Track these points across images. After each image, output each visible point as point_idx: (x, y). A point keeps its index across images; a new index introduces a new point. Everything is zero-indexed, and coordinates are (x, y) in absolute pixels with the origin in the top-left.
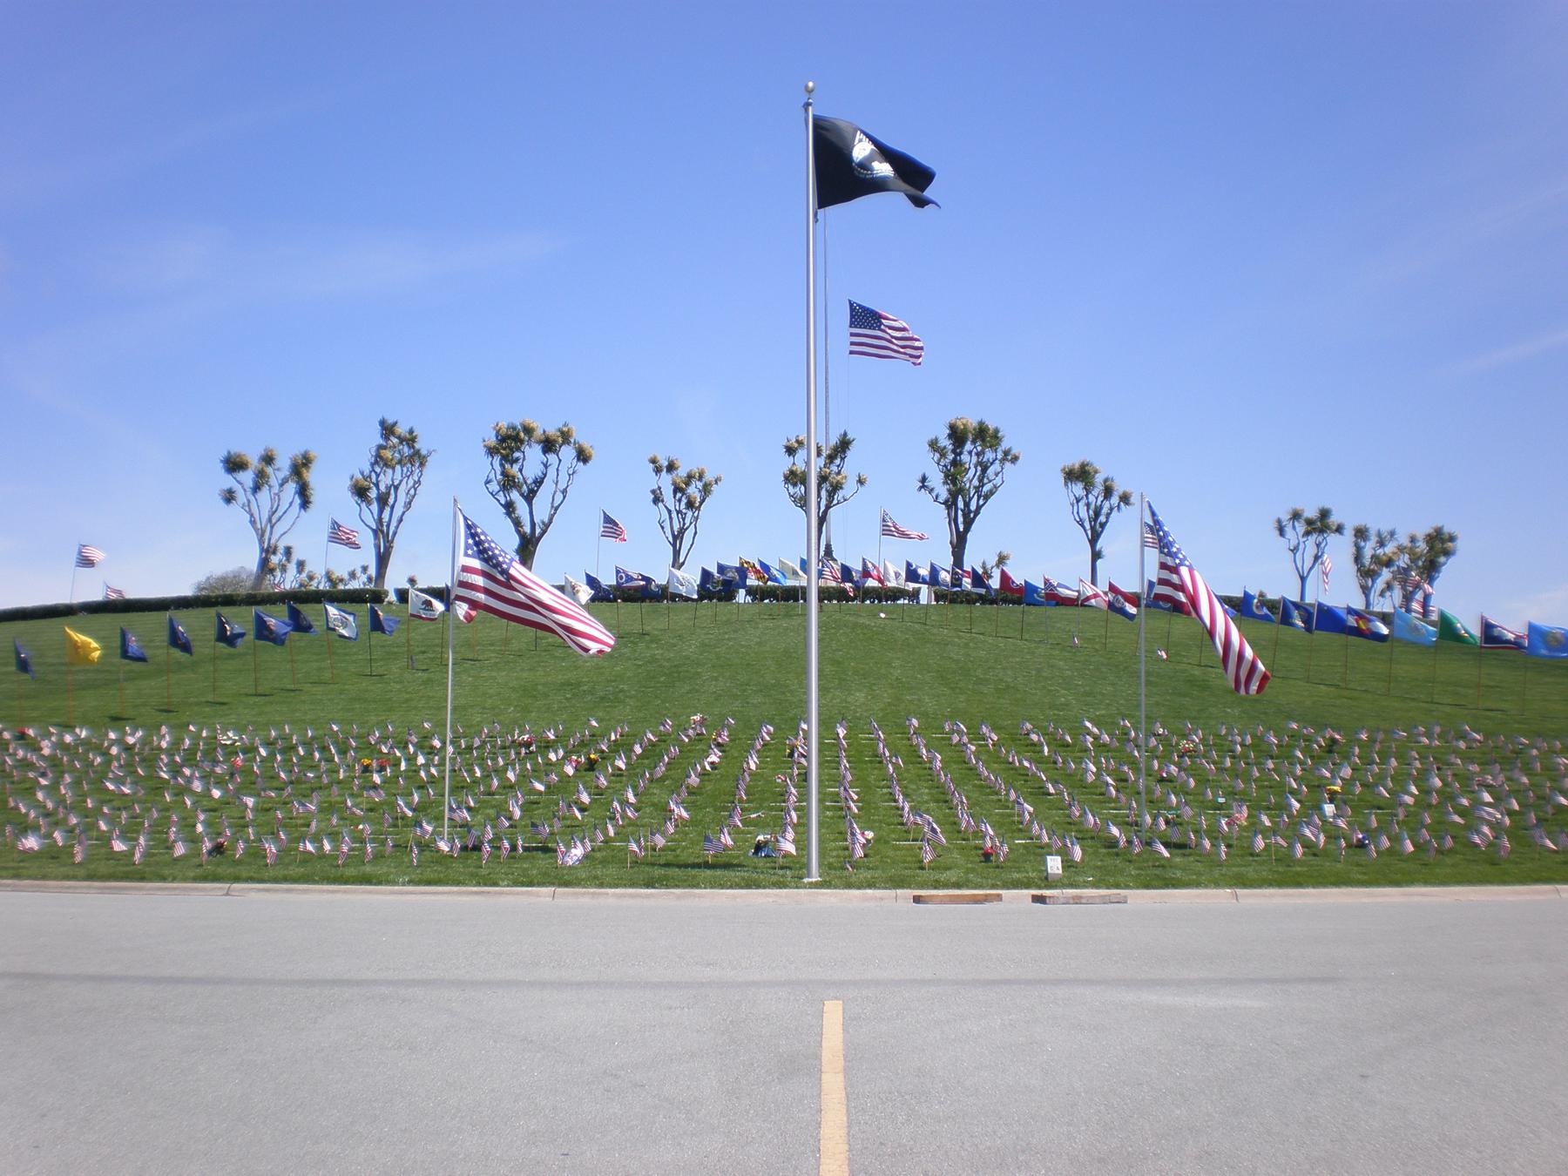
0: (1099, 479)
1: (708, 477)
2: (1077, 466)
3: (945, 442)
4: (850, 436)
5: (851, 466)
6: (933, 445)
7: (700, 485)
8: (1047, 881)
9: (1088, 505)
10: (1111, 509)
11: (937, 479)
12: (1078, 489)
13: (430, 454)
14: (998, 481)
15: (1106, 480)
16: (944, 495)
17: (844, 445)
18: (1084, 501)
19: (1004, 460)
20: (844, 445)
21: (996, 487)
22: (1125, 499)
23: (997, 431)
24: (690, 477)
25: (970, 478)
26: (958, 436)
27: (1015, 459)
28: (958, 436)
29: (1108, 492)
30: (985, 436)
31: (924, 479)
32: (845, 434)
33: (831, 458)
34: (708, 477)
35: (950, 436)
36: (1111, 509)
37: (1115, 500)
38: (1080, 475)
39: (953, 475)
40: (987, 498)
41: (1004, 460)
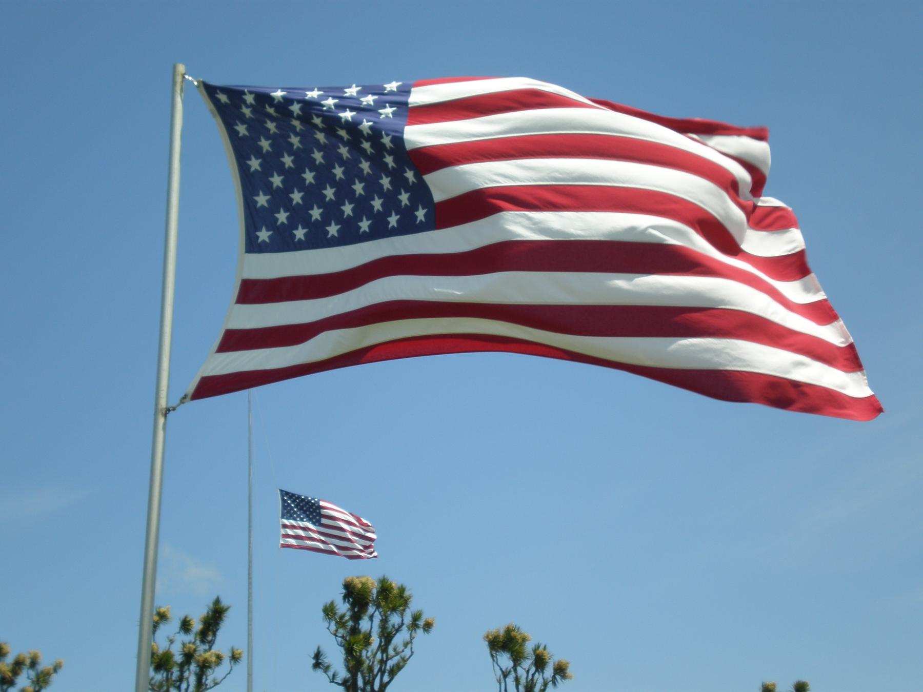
0: (529, 647)
1: (45, 664)
2: (502, 632)
3: (343, 608)
4: (224, 603)
5: (227, 638)
6: (329, 611)
7: (32, 673)
8: (299, 102)
9: (517, 680)
10: (545, 685)
11: (336, 658)
12: (505, 660)
13: (57, 668)
14: (407, 652)
15: (535, 651)
16: (343, 674)
17: (215, 618)
18: (513, 675)
19: (414, 625)
20: (215, 618)
21: (405, 660)
22: (560, 670)
23: (402, 590)
24: (18, 665)
25: (370, 654)
26: (356, 596)
27: (428, 626)
28: (356, 596)
29: (540, 662)
30: (391, 598)
31: (317, 656)
32: (217, 601)
33: (203, 634)
34: (45, 664)
35: (346, 597)
36: (545, 685)
37: (549, 672)
38: (506, 643)
39: (353, 644)
40: (393, 672)
41: (414, 625)
